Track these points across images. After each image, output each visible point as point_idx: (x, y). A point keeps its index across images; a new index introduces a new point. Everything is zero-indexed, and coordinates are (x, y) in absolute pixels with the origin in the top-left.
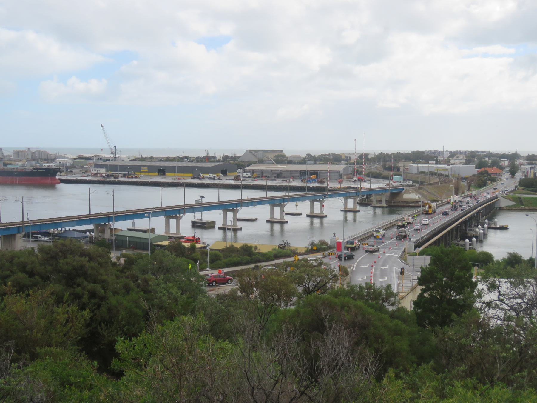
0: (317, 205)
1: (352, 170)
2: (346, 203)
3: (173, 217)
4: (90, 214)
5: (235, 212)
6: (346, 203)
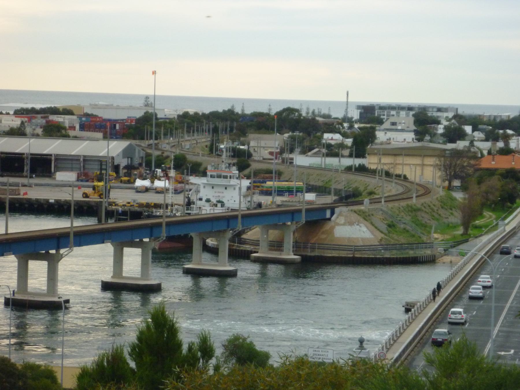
0: (38, 269)
1: (143, 154)
2: (23, 274)
3: (38, 257)
4: (7, 234)
5: (53, 262)
6: (23, 274)
